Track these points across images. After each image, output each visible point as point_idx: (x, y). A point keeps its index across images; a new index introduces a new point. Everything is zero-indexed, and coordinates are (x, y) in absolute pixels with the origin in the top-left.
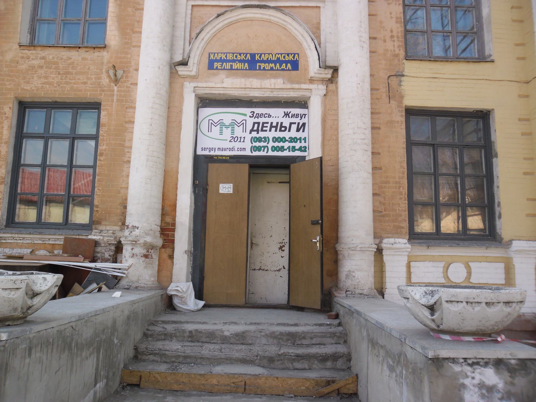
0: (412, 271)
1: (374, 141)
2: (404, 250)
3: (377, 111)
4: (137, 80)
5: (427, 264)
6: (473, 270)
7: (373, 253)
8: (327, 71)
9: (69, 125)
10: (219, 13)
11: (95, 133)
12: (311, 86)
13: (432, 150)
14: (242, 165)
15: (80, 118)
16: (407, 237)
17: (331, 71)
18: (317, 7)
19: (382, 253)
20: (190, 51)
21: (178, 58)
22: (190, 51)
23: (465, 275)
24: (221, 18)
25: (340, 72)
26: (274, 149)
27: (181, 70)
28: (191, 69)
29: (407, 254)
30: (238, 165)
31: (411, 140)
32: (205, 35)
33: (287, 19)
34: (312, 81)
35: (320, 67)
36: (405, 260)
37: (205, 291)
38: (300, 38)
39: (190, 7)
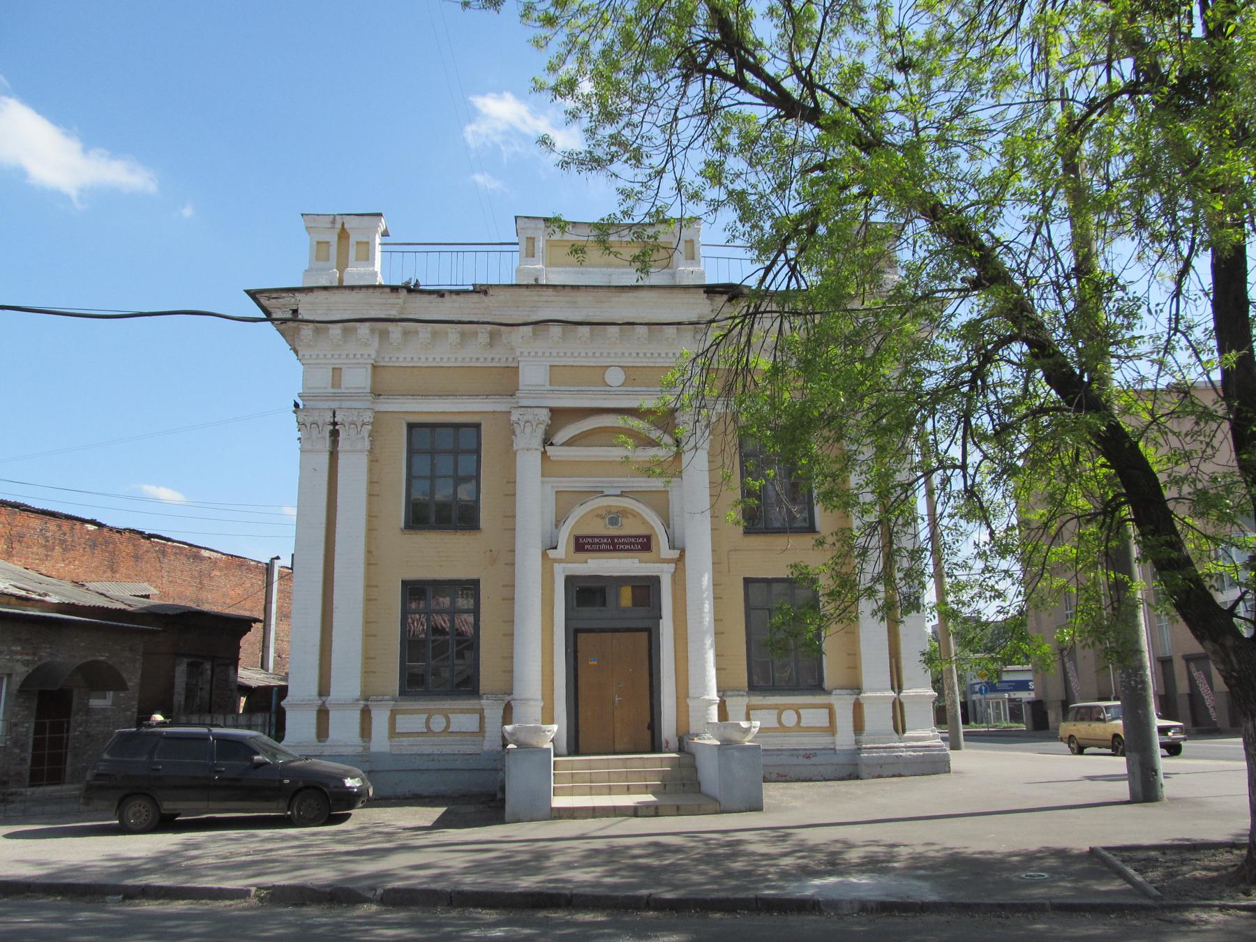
6: (803, 716)
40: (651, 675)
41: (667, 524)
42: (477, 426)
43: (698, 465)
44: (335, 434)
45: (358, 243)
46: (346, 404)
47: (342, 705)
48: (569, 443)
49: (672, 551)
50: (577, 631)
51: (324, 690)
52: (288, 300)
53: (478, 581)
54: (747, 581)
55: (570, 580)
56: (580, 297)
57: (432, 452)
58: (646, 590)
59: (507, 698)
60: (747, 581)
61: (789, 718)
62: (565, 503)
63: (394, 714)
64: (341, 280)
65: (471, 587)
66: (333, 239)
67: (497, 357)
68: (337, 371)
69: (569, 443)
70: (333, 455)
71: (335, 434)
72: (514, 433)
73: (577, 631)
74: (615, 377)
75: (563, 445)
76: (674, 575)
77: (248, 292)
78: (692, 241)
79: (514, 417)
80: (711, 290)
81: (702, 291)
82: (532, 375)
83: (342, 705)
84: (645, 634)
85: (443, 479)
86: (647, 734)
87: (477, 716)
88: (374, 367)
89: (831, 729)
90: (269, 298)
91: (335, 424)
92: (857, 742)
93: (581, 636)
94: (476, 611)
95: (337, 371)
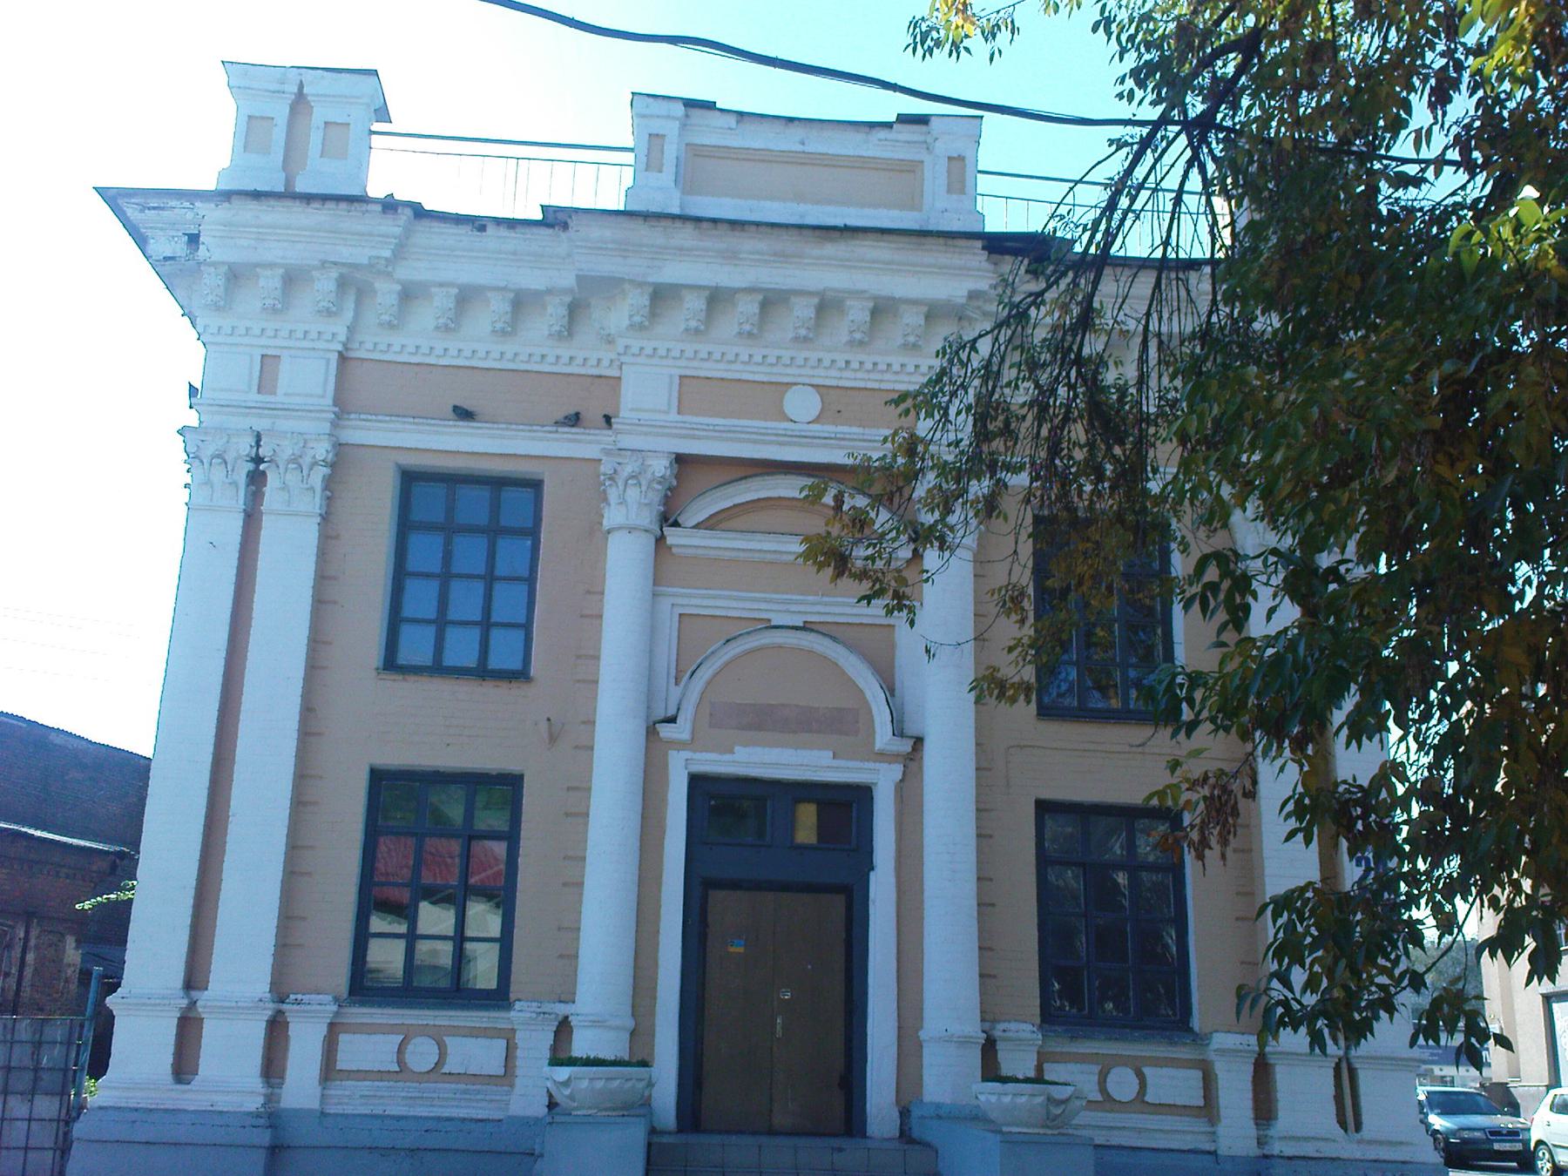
1: (981, 862)
6: (1149, 1081)
8: (905, 741)
11: (530, 525)
16: (1038, 1021)
17: (911, 742)
21: (661, 714)
23: (1136, 1088)
24: (733, 644)
26: (479, 1092)
27: (666, 731)
32: (705, 674)
34: (883, 756)
39: (676, 618)
41: (890, 689)
42: (536, 485)
44: (257, 479)
46: (285, 425)
47: (231, 1010)
48: (709, 524)
50: (710, 884)
51: (194, 979)
52: (182, 213)
53: (521, 777)
54: (1044, 808)
55: (697, 782)
56: (748, 244)
57: (449, 529)
58: (845, 808)
59: (562, 1009)
60: (1044, 808)
61: (1123, 1084)
62: (691, 642)
63: (334, 1030)
64: (289, 181)
65: (508, 786)
66: (281, 111)
67: (580, 355)
68: (269, 363)
70: (252, 520)
71: (257, 479)
72: (605, 500)
73: (710, 884)
74: (802, 405)
75: (696, 527)
77: (114, 198)
78: (961, 158)
79: (606, 468)
80: (998, 245)
81: (979, 244)
82: (646, 393)
83: (231, 1010)
84: (840, 900)
85: (456, 551)
88: (343, 359)
89: (1208, 1109)
90: (144, 208)
91: (258, 460)
92: (1261, 1142)
93: (717, 897)
94: (512, 837)
95: (269, 363)
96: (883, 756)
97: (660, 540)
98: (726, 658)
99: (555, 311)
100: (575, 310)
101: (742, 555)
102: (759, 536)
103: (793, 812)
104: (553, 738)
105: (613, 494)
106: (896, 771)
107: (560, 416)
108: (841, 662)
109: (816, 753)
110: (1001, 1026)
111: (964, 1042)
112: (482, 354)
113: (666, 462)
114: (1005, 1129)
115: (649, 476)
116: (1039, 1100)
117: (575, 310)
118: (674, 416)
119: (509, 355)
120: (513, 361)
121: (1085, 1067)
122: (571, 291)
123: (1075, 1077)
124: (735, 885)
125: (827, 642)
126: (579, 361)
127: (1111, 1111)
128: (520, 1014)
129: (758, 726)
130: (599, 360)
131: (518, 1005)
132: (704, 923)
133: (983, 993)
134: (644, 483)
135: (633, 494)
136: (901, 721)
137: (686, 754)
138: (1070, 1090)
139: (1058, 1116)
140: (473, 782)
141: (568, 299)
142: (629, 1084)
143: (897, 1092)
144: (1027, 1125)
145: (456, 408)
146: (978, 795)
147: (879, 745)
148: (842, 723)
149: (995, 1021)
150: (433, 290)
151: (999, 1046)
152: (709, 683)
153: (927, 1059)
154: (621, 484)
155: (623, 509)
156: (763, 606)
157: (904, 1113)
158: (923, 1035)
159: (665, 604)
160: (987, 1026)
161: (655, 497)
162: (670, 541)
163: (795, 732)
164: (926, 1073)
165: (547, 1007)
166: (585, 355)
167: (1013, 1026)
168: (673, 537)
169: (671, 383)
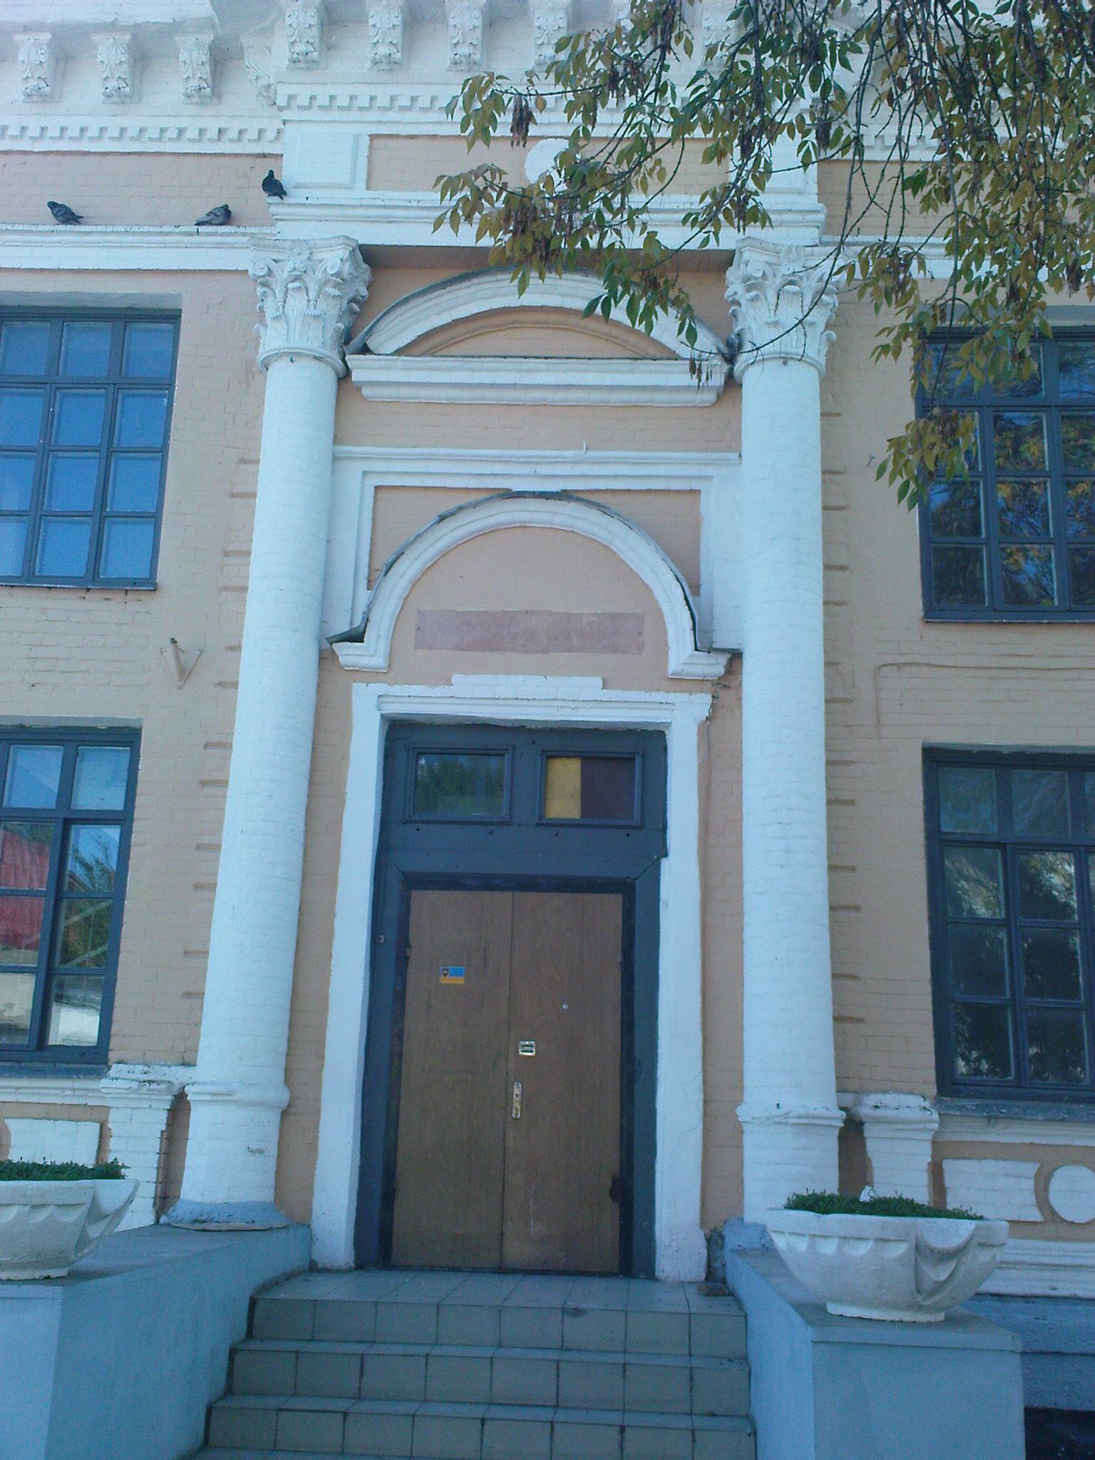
0: (948, 1183)
2: (921, 1126)
3: (847, 757)
4: (237, 672)
5: (990, 1166)
7: (836, 1132)
8: (714, 658)
9: (52, 782)
10: (443, 511)
12: (672, 697)
13: (1000, 858)
14: (497, 894)
15: (82, 760)
16: (933, 1090)
17: (723, 659)
18: (691, 491)
19: (862, 1132)
20: (369, 608)
21: (343, 627)
22: (369, 608)
24: (449, 524)
25: (749, 663)
27: (348, 654)
28: (372, 652)
29: (929, 1136)
30: (487, 894)
31: (941, 833)
32: (408, 569)
33: (616, 526)
34: (680, 683)
35: (696, 649)
36: (924, 1155)
37: (396, 1229)
38: (647, 577)
39: (370, 492)
40: (628, 1026)
41: (692, 586)
43: (780, 402)
45: (368, 189)
48: (425, 345)
49: (702, 657)
54: (938, 760)
55: (401, 735)
58: (623, 764)
59: (178, 1075)
60: (938, 760)
69: (425, 345)
75: (399, 352)
76: (707, 728)
84: (613, 903)
86: (609, 1216)
87: (94, 1128)
93: (424, 900)
96: (680, 683)
97: (344, 376)
98: (441, 545)
99: (192, 54)
100: (222, 60)
101: (467, 394)
102: (488, 364)
103: (544, 773)
104: (184, 673)
105: (270, 309)
106: (701, 704)
107: (202, 214)
108: (617, 546)
109: (576, 680)
110: (871, 1099)
111: (807, 1124)
112: (94, 132)
113: (345, 254)
114: (833, 1309)
115: (319, 275)
116: (900, 1249)
117: (222, 60)
118: (360, 193)
119: (132, 132)
120: (138, 139)
121: (1011, 1166)
122: (207, 24)
123: (992, 1187)
124: (450, 882)
125: (594, 515)
126: (233, 134)
127: (1058, 1238)
128: (113, 1085)
129: (490, 645)
130: (261, 132)
131: (115, 1070)
132: (403, 943)
133: (839, 1047)
134: (313, 287)
135: (297, 304)
136: (710, 632)
137: (381, 688)
138: (967, 1227)
139: (938, 1287)
140: (74, 739)
141: (208, 38)
142: (42, 1215)
143: (703, 1205)
144: (872, 1304)
145: (53, 205)
146: (829, 739)
147: (673, 666)
148: (616, 636)
149: (860, 1092)
150: (18, 38)
151: (869, 1131)
152: (415, 583)
153: (751, 1153)
154: (278, 289)
155: (281, 326)
156: (498, 469)
157: (714, 1241)
158: (743, 1112)
159: (352, 474)
160: (848, 1099)
161: (331, 309)
162: (356, 376)
163: (545, 651)
164: (748, 1174)
165: (158, 1072)
166: (240, 121)
167: (890, 1099)
168: (362, 369)
169: (356, 147)
